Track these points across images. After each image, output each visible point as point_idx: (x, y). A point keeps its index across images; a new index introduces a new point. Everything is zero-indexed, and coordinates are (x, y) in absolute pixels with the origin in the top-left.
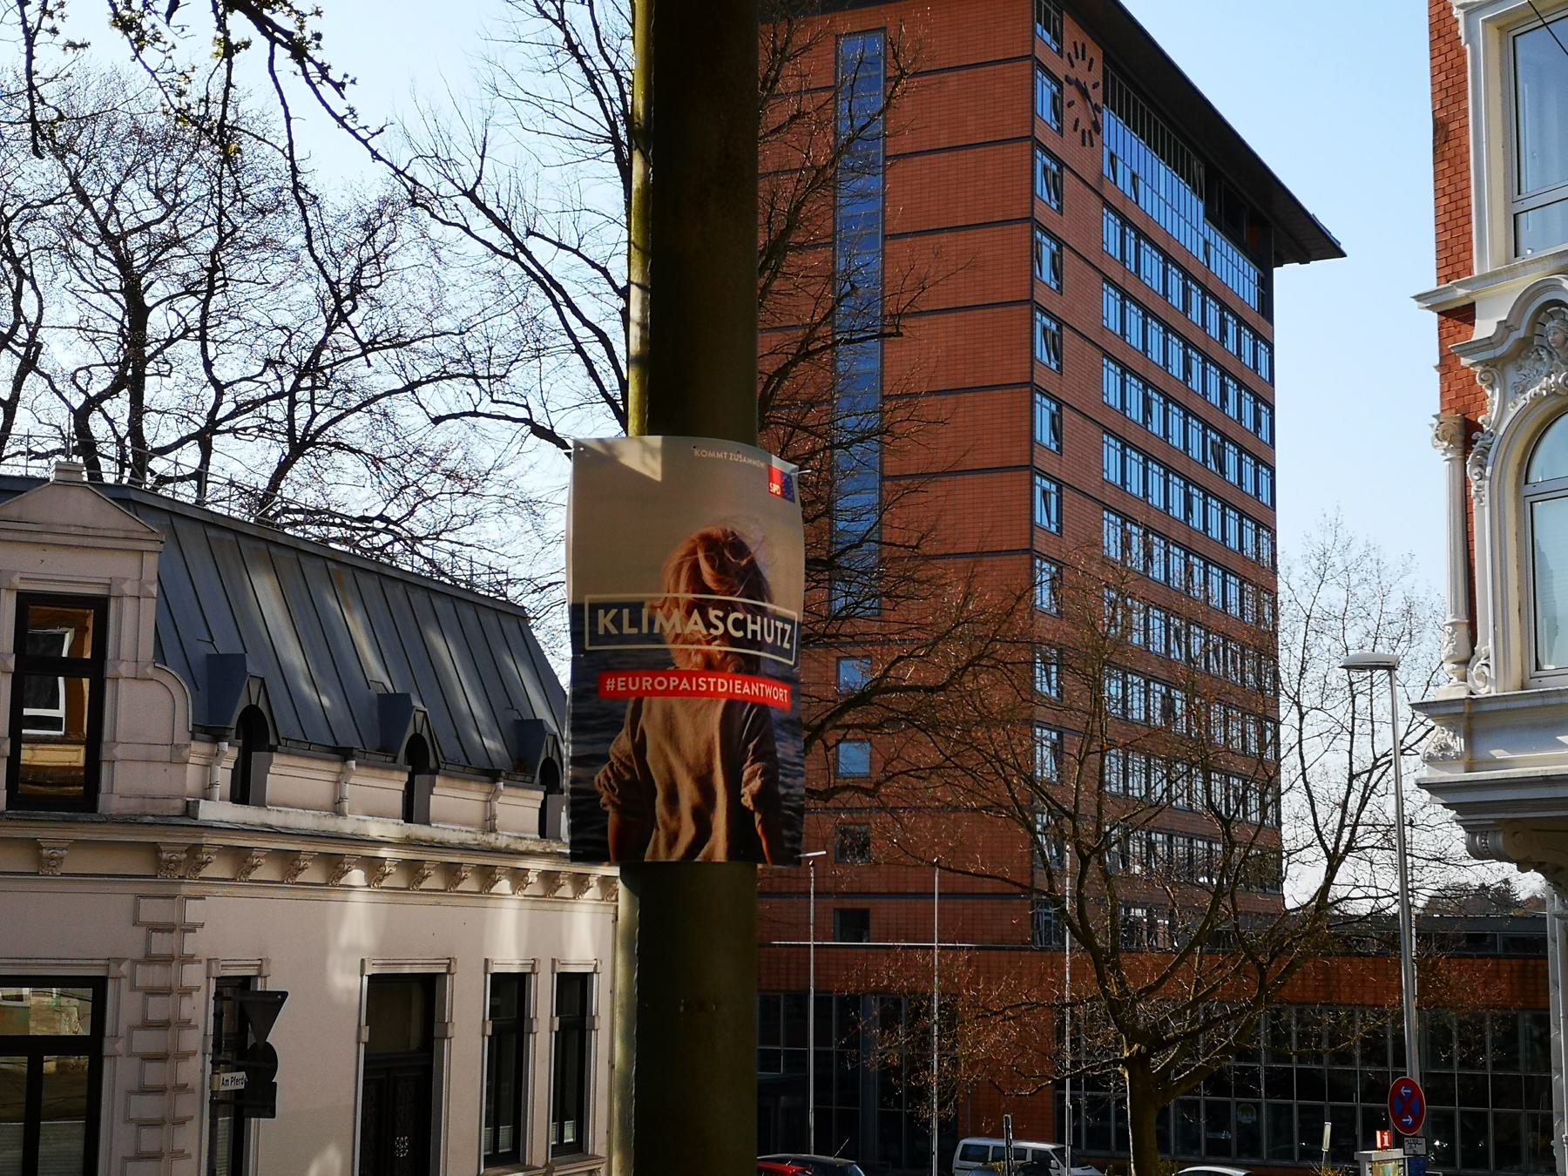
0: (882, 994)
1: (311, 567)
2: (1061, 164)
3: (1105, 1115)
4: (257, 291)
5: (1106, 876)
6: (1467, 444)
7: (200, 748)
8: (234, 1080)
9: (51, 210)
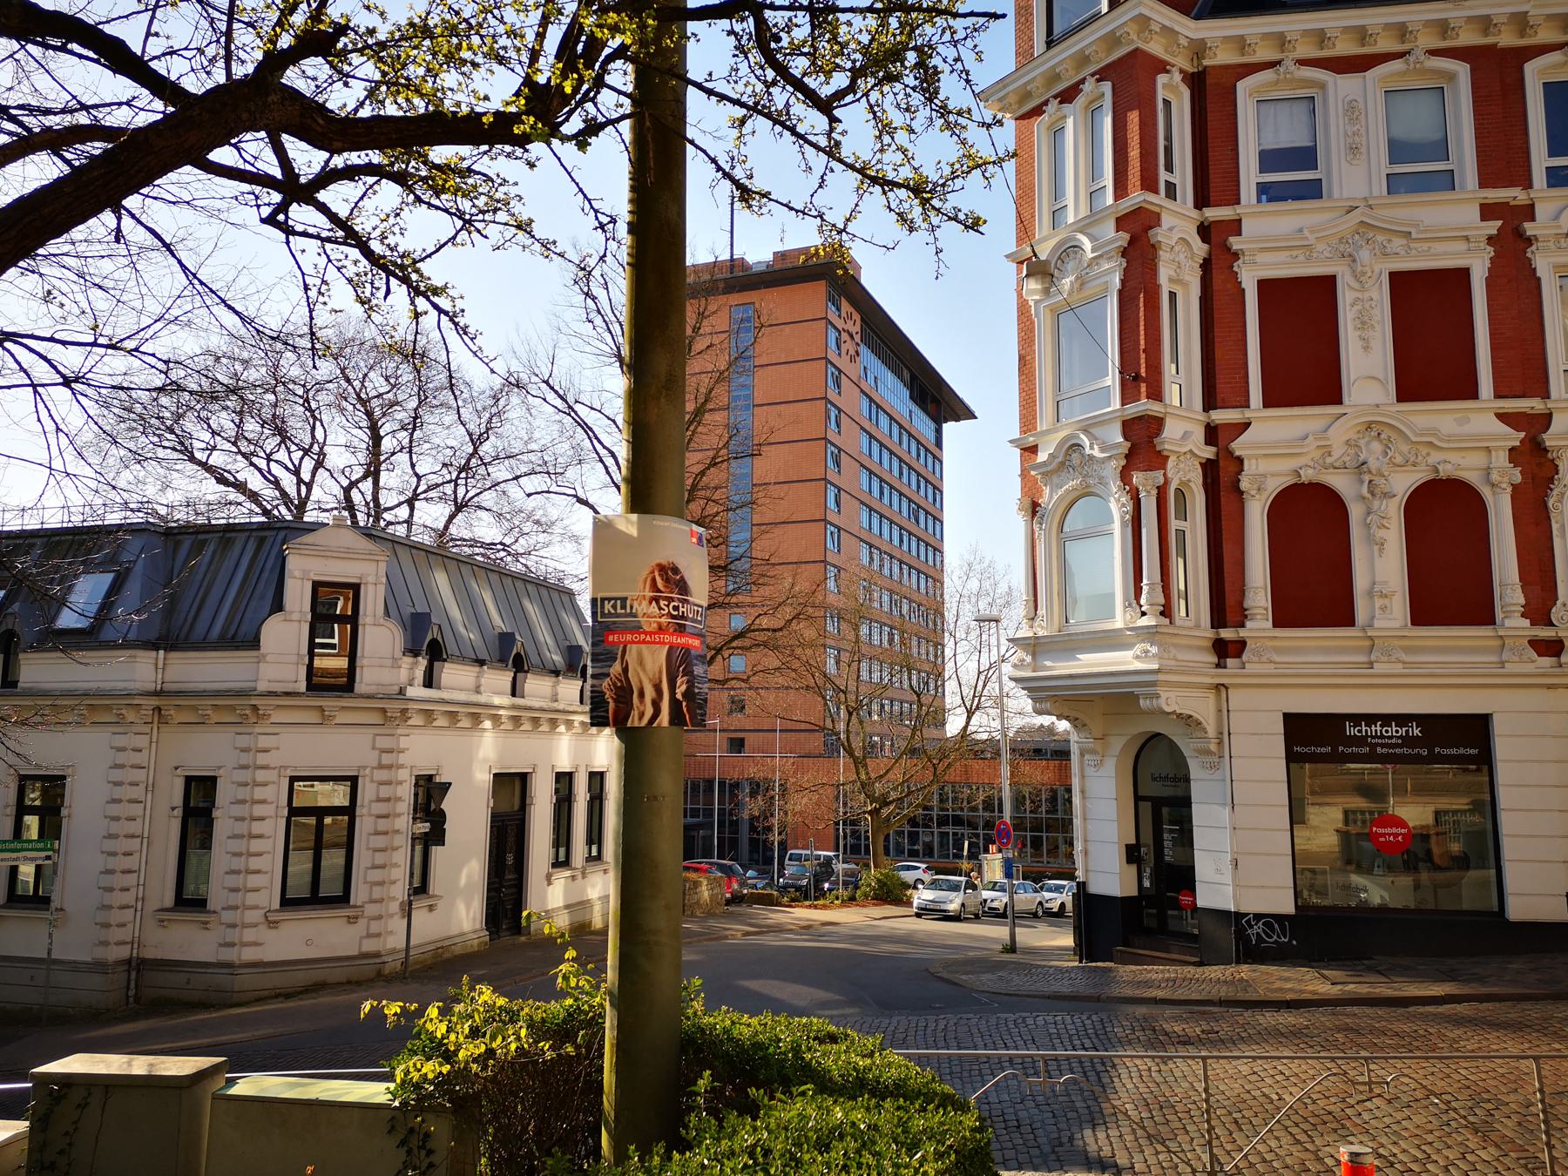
0: (751, 781)
1: (465, 569)
2: (840, 371)
3: (859, 838)
4: (439, 429)
5: (861, 722)
6: (1034, 513)
7: (408, 660)
8: (425, 827)
9: (330, 386)
